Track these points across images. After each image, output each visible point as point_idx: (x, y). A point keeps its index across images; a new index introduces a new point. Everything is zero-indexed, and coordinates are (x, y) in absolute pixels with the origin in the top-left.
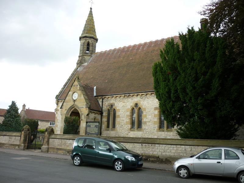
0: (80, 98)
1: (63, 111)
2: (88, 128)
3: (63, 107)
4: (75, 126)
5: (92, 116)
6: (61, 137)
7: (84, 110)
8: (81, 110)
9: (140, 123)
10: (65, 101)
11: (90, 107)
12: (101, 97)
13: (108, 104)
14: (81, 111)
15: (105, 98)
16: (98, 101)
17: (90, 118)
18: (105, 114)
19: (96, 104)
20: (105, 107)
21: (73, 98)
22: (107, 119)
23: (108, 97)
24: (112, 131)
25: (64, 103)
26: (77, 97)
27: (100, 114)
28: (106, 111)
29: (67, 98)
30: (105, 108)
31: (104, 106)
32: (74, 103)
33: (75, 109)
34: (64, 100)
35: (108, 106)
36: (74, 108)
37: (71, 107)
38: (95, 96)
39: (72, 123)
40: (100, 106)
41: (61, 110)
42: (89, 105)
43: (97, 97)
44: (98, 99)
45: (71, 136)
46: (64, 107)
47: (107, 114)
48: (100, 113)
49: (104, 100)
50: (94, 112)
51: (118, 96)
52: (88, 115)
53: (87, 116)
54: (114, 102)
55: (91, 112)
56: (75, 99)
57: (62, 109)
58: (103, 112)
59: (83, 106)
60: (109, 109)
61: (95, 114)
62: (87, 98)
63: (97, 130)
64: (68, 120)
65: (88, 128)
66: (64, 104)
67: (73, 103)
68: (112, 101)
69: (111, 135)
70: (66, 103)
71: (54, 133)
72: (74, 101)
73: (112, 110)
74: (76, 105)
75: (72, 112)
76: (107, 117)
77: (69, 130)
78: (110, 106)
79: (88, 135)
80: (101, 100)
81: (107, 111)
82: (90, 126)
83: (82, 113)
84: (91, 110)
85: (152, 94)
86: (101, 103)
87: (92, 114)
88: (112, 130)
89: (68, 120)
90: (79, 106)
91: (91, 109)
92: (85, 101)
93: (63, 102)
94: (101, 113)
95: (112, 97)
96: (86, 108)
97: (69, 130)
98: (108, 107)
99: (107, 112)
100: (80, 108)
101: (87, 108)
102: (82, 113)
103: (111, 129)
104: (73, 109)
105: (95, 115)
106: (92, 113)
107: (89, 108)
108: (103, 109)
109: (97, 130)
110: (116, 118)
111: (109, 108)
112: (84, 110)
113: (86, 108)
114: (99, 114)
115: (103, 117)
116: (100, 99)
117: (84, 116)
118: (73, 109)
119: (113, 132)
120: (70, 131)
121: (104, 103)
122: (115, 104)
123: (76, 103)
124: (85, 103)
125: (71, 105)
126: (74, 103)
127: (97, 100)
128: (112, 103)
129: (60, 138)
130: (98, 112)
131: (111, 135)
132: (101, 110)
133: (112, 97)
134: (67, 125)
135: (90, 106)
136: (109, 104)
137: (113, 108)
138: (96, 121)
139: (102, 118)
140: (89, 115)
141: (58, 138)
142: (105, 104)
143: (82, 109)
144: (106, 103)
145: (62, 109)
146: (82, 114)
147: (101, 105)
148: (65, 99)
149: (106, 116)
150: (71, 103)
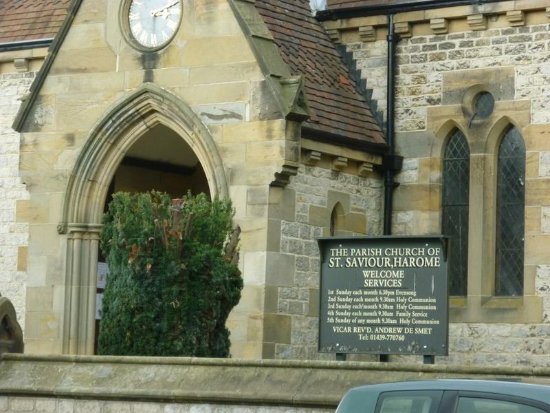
0: (199, 31)
1: (45, 148)
2: (341, 303)
3: (37, 117)
4: (207, 282)
5: (316, 186)
6: (99, 382)
7: (242, 143)
8: (216, 137)
9: (515, 249)
10: (59, 62)
11: (300, 112)
12: (382, 20)
13: (447, 80)
14: (218, 152)
15: (419, 32)
16: (348, 60)
17: (299, 206)
18: (419, 170)
19: (334, 81)
20: (422, 112)
21: (136, 29)
22: (437, 215)
23: (449, 20)
24: (489, 321)
25: (51, 79)
26: (173, 26)
27: (379, 172)
28: (432, 145)
29: (78, 36)
30: (420, 116)
31: (404, 100)
32: (149, 77)
33: (160, 129)
34: (44, 52)
35: (449, 96)
36: (151, 120)
37: (122, 118)
38: (323, 17)
39: (185, 252)
40: (372, 104)
41: (22, 145)
42: (293, 91)
43: (338, 24)
44: (350, 42)
45: (196, 372)
46: (47, 114)
47: (437, 175)
48: (379, 161)
49: (405, 49)
50: (328, 158)
51: (11, 61)
52: (281, 181)
53: (278, 195)
54: (506, 60)
55: (306, 152)
56: (148, 39)
57: (29, 137)
58: (402, 147)
59: (231, 106)
60: (455, 131)
61: (336, 173)
62: (264, 31)
63: (431, 315)
64: (146, 227)
65: (341, 303)
66: (53, 86)
67: (141, 73)
68: (484, 52)
69: (481, 356)
70: (66, 77)
71: (18, 346)
72: (149, 58)
73: (491, 136)
74: (162, 96)
75: (129, 162)
76: (437, 199)
77: (158, 318)
78: (468, 99)
79: (341, 356)
80: (380, 47)
81: (440, 142)
82: (353, 279)
83: (230, 162)
84: (308, 134)
85: (417, 29)
86: (376, 80)
87: (316, 170)
88: (493, 314)
89: (146, 227)
90: (198, 107)
91: (305, 124)
92: (253, 60)
93: (37, 67)
94: (386, 165)
95: (488, 16)
96: (263, 117)
97: (158, 318)
98: (450, 111)
99: (438, 154)
100: (208, 122)
101: (279, 124)
102: (230, 162)
103: (484, 301)
104: (140, 129)
105: (337, 184)
106: (313, 164)
107: (292, 118)
108: (398, 130)
109: (431, 315)
110: (528, 209)
111: (460, 121)
112: (242, 143)
113: (263, 117)
114: (365, 176)
115: (398, 196)
116: (369, 37)
117: (253, 192)
118: (140, 129)
119: (504, 329)
120: (164, 325)
121: (405, 79)
122: (519, 82)
123: (164, 76)
124: (257, 77)
125: (119, 98)
126: (149, 77)
127: (342, 48)
128: (486, 74)
129: (97, 390)
130: (358, 156)
131: (481, 356)
132: (379, 139)
133: (488, 16)
134: (139, 277)
135: (300, 102)
136: (456, 86)
137: (498, 115)
138: (343, 233)
139: (397, 203)
140: (295, 184)
141: (74, 389)
142: (420, 79)
143: (225, 134)
144: (432, 77)
145: (37, 128)
146: (230, 177)
147: (380, 96)
148: (56, 47)
149: (430, 189)
150: (118, 83)
